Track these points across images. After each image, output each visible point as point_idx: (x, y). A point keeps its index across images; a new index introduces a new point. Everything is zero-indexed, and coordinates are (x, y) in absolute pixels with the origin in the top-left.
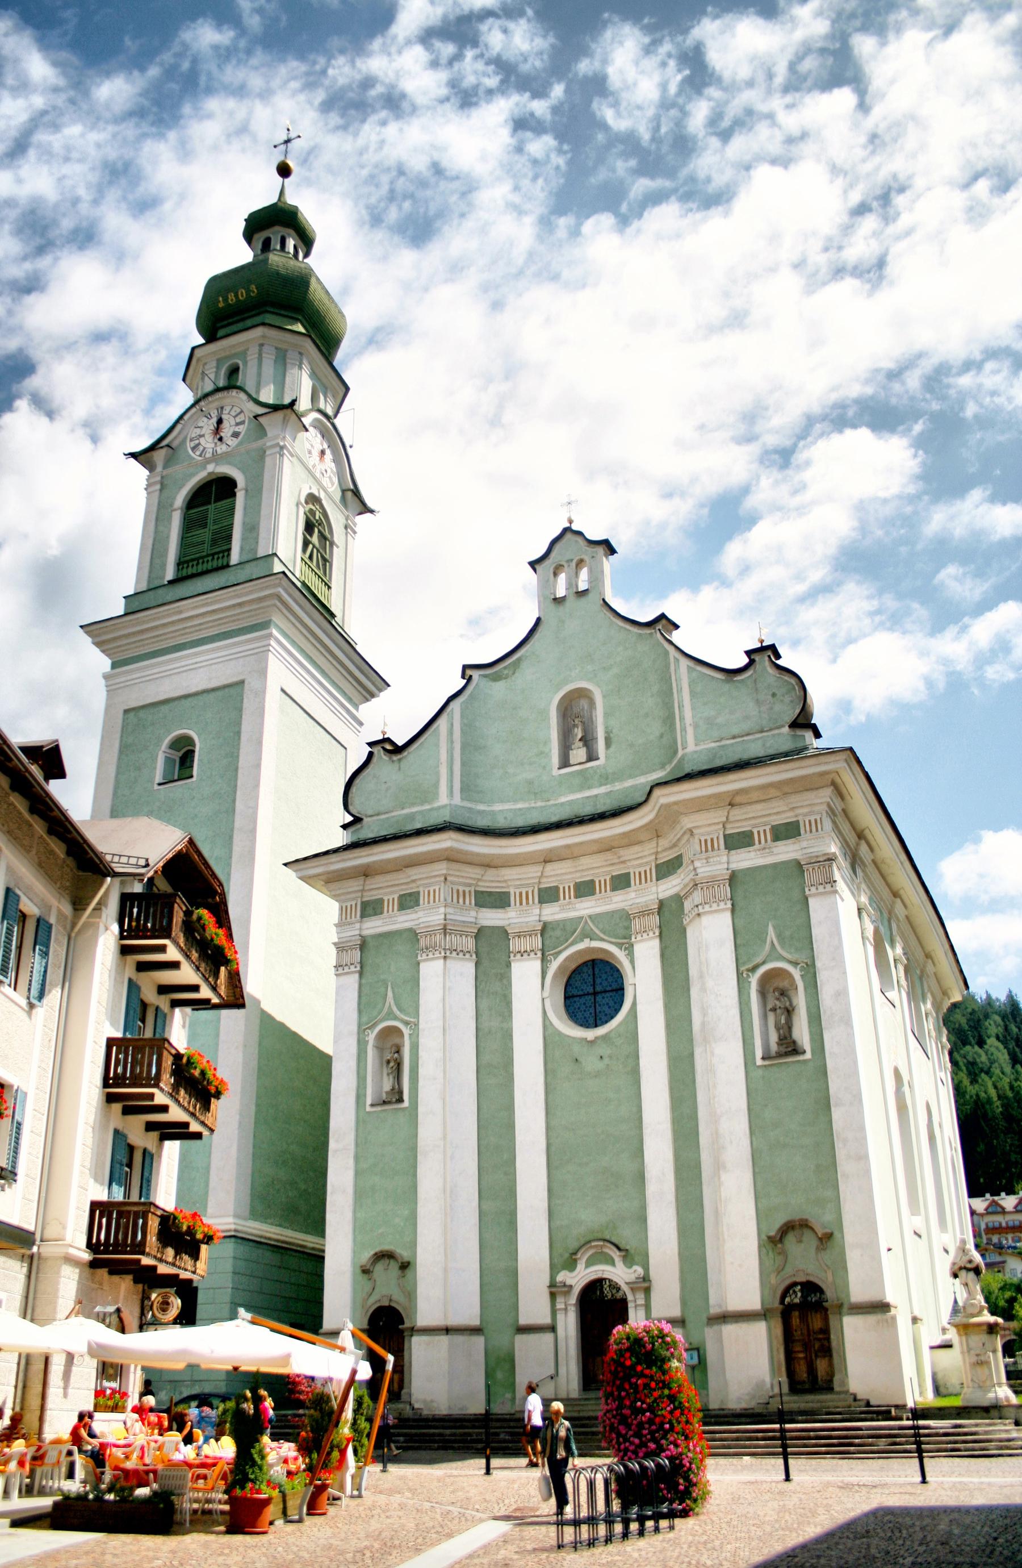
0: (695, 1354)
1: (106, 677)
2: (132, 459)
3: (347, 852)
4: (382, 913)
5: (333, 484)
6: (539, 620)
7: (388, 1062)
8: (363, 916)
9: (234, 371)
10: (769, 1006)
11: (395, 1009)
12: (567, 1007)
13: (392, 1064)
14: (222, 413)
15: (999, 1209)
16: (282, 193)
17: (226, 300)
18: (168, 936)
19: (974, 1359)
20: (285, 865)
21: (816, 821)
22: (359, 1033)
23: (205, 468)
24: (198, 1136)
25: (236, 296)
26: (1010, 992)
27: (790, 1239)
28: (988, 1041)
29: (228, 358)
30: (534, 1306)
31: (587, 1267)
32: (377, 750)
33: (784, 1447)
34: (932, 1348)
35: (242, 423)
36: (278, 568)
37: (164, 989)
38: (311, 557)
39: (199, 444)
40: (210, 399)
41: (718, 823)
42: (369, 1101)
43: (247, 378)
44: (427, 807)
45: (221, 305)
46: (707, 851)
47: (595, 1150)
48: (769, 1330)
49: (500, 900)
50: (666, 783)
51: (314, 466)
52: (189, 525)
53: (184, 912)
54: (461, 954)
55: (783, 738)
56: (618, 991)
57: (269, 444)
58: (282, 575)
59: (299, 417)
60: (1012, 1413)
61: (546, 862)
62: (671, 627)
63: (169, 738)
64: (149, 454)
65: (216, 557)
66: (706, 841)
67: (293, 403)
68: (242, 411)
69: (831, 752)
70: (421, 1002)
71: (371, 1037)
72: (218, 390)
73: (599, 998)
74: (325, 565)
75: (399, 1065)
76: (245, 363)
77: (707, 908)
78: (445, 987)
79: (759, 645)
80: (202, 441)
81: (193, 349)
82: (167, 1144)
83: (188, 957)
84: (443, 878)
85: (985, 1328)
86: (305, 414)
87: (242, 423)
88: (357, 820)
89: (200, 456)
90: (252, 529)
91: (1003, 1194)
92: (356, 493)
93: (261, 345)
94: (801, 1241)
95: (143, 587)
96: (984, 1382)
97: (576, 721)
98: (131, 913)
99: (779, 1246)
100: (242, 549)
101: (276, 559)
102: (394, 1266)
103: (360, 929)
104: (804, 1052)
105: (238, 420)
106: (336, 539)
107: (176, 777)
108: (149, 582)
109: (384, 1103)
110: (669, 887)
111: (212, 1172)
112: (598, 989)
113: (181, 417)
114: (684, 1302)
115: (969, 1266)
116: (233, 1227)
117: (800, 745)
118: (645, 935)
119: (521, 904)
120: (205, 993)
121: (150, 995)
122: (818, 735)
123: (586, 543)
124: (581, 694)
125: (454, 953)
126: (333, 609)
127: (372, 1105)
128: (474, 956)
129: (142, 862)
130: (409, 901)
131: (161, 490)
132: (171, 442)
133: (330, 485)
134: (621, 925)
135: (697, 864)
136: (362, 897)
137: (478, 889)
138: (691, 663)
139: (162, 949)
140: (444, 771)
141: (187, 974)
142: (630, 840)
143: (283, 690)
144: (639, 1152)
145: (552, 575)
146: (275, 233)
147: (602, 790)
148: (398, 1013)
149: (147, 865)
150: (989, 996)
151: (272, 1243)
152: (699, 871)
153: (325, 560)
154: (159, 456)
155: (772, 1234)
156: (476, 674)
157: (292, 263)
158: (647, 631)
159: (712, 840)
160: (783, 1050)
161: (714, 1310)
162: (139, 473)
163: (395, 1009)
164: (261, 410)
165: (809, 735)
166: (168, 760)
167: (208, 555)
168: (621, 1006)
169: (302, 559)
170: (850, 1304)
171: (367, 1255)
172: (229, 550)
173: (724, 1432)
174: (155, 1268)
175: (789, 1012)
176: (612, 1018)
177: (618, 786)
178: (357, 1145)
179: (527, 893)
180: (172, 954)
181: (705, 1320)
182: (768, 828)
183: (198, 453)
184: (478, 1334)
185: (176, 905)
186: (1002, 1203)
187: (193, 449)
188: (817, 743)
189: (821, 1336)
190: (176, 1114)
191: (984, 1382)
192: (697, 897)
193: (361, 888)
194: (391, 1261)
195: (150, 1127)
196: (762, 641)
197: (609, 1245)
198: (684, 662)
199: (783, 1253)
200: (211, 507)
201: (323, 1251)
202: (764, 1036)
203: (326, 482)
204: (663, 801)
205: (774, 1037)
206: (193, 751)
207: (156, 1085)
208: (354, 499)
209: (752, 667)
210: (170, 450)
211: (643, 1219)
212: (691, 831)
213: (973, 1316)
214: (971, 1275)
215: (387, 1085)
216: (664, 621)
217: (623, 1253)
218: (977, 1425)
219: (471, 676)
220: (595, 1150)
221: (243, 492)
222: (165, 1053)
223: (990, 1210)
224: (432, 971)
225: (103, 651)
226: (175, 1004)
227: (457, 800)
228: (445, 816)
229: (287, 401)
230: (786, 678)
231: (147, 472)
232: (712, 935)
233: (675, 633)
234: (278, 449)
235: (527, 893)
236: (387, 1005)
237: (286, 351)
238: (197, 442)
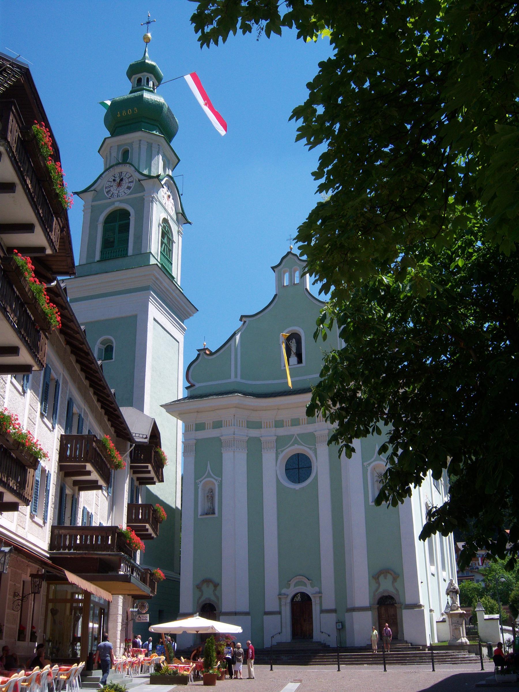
0: (340, 624)
6: (276, 295)
12: (287, 474)
13: (209, 497)
17: (121, 114)
18: (150, 462)
19: (454, 628)
20: (161, 406)
26: (296, 142)
30: (271, 604)
32: (202, 353)
33: (384, 660)
34: (437, 622)
35: (132, 182)
39: (110, 190)
42: (199, 514)
49: (258, 425)
56: (309, 468)
60: (468, 648)
68: (132, 176)
78: (234, 464)
80: (112, 189)
81: (105, 139)
87: (132, 182)
88: (192, 386)
92: (183, 214)
100: (134, 247)
101: (151, 255)
102: (211, 586)
106: (174, 239)
109: (206, 514)
112: (300, 466)
126: (173, 275)
143: (155, 319)
146: (144, 75)
156: (247, 319)
164: (142, 178)
166: (100, 350)
170: (406, 605)
173: (355, 655)
176: (306, 479)
183: (110, 195)
187: (107, 192)
197: (304, 578)
203: (170, 211)
210: (96, 193)
217: (310, 582)
218: (453, 652)
224: (227, 456)
238: (109, 189)
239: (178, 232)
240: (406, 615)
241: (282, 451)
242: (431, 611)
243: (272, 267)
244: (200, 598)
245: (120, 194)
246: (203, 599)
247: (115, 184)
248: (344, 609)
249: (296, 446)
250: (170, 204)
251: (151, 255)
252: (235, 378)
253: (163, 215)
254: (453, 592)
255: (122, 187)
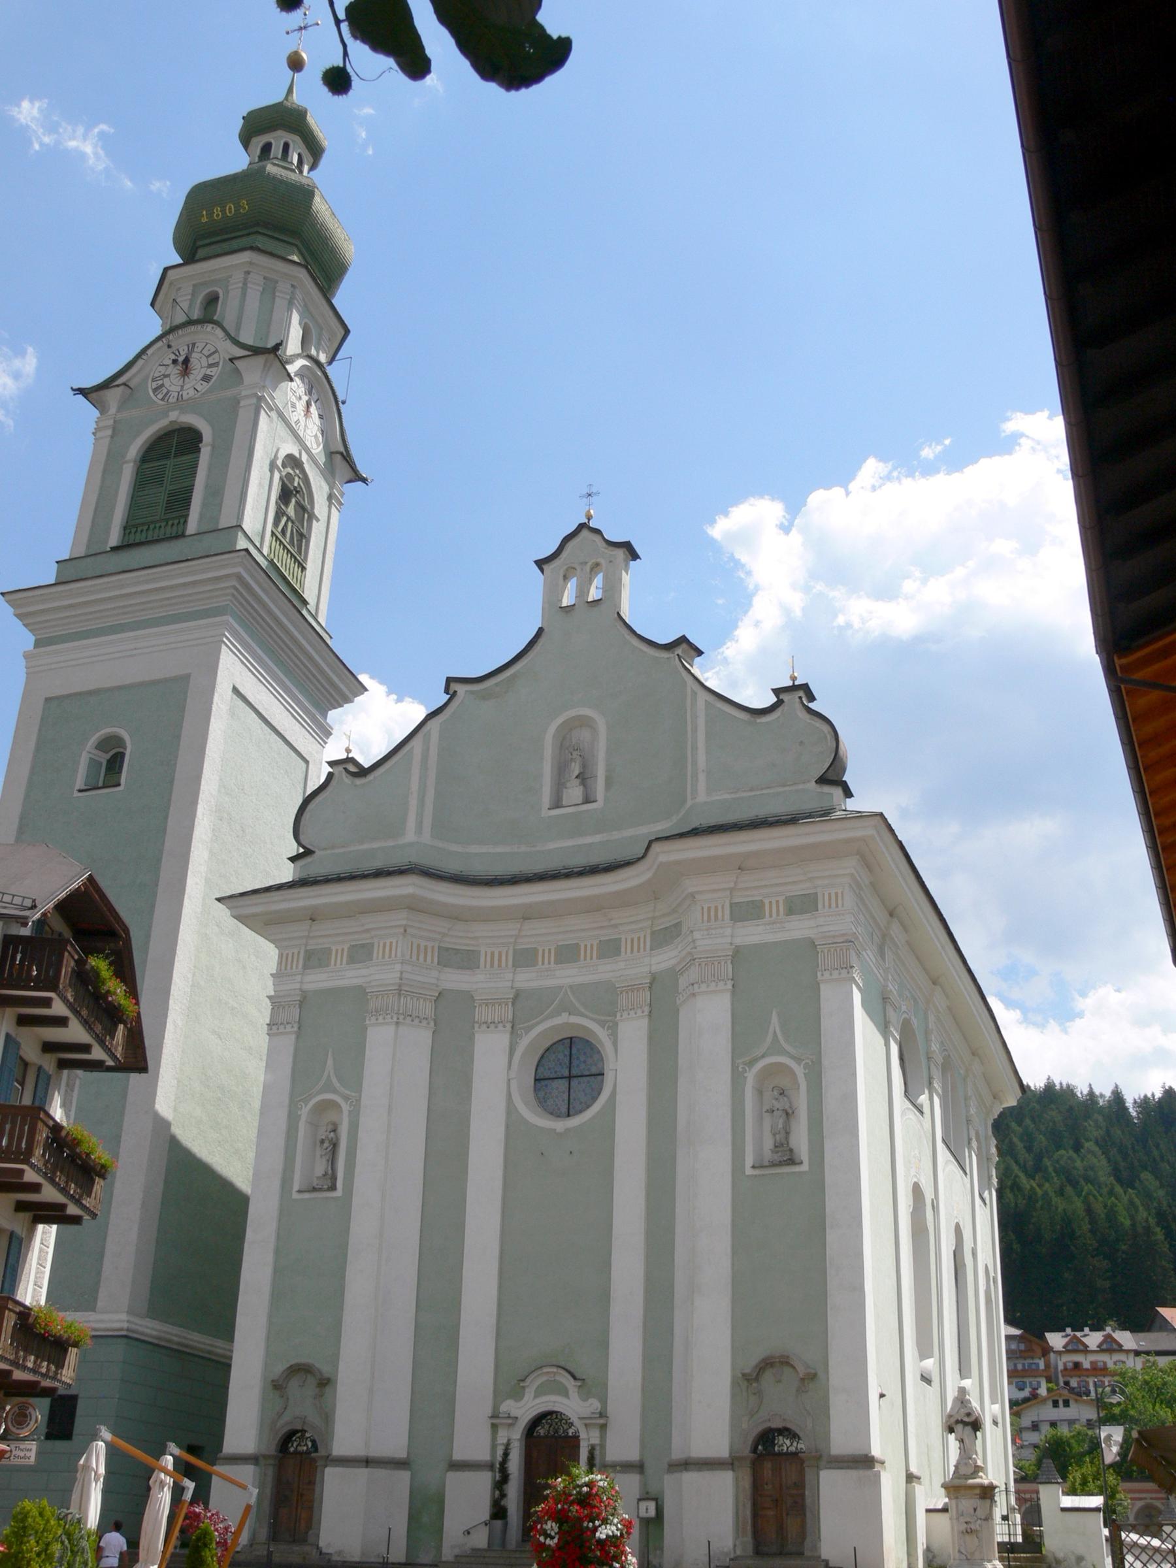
0: (652, 1506)
1: (27, 656)
2: (80, 396)
3: (291, 891)
4: (328, 965)
5: (318, 446)
6: (541, 630)
7: (322, 1142)
8: (305, 967)
9: (212, 301)
10: (766, 1108)
11: (334, 1080)
13: (326, 1144)
14: (193, 350)
15: (1081, 1348)
16: (290, 90)
17: (210, 214)
18: (54, 988)
20: (219, 900)
21: (837, 894)
22: (290, 1106)
23: (168, 416)
24: (76, 1220)
25: (223, 211)
26: (1117, 1086)
27: (768, 1377)
28: (1087, 1145)
29: (205, 284)
31: (535, 1397)
34: (928, 1511)
35: (216, 365)
36: (242, 544)
37: (48, 1047)
38: (283, 532)
39: (162, 385)
40: (180, 332)
41: (724, 889)
42: (296, 1187)
43: (227, 311)
44: (391, 843)
45: (204, 220)
46: (709, 921)
47: (556, 1257)
48: (736, 1480)
49: (467, 960)
50: (667, 838)
51: (297, 422)
52: (142, 482)
53: (76, 961)
54: (417, 1020)
55: (811, 795)
57: (244, 393)
58: (244, 553)
59: (283, 364)
61: (525, 918)
62: (693, 653)
63: (98, 735)
64: (102, 393)
65: (170, 523)
66: (709, 908)
67: (277, 347)
69: (860, 816)
70: (366, 1073)
71: (305, 1112)
72: (190, 322)
73: (574, 1082)
74: (300, 541)
75: (335, 1145)
76: (227, 292)
77: (704, 987)
78: (394, 1060)
79: (791, 684)
81: (166, 270)
82: (40, 1227)
83: (77, 1013)
84: (402, 930)
85: (978, 1491)
86: (291, 360)
87: (216, 365)
88: (308, 852)
89: (162, 399)
90: (215, 493)
91: (1087, 1329)
92: (347, 457)
93: (248, 273)
94: (779, 1381)
95: (81, 551)
96: (973, 1554)
97: (575, 753)
98: (14, 958)
99: (754, 1385)
100: (202, 516)
101: (240, 534)
102: (311, 1381)
103: (301, 982)
104: (801, 1163)
105: (211, 361)
106: (316, 512)
107: (101, 784)
108: (88, 547)
109: (314, 1190)
110: (664, 959)
111: (105, 1259)
112: (574, 1072)
113: (144, 351)
114: (643, 1445)
115: (966, 1419)
116: (125, 1325)
117: (825, 805)
118: (632, 1012)
119: (492, 965)
120: (97, 1053)
121: (31, 1052)
122: (848, 794)
123: (604, 544)
124: (583, 722)
125: (409, 1019)
127: (299, 1191)
128: (432, 1024)
129: (28, 903)
130: (360, 953)
131: (112, 437)
132: (129, 380)
133: (315, 446)
134: (605, 1001)
135: (697, 935)
136: (306, 945)
137: (442, 945)
138: (711, 698)
139: (47, 1003)
140: (413, 803)
141: (76, 1032)
142: (624, 900)
143: (235, 690)
144: (606, 1266)
145: (561, 578)
146: (277, 139)
147: (597, 838)
148: (337, 1085)
149: (34, 907)
150: (1091, 1093)
151: (175, 1347)
152: (698, 943)
153: (301, 535)
154: (113, 396)
155: (747, 1371)
156: (461, 689)
157: (293, 177)
158: (664, 655)
159: (716, 908)
160: (777, 1157)
161: (677, 1454)
162: (88, 413)
163: (334, 1080)
165: (838, 792)
167: (161, 520)
168: (599, 1094)
169: (273, 533)
171: (280, 1368)
172: (187, 516)
174: (9, 1373)
175: (788, 1114)
176: (588, 1107)
177: (616, 835)
178: (278, 1238)
179: (500, 953)
180: (59, 1008)
181: (666, 1466)
182: (781, 899)
183: (160, 396)
184: (405, 1469)
185: (66, 954)
186: (1084, 1340)
187: (155, 390)
188: (851, 805)
189: (794, 1492)
190: (49, 1194)
191: (973, 1554)
192: (693, 974)
193: (306, 933)
194: (304, 1378)
195: (21, 1207)
196: (794, 679)
198: (703, 696)
199: (759, 1393)
200: (170, 463)
201: (231, 1358)
202: (758, 1141)
203: (311, 442)
204: (662, 858)
205: (768, 1143)
206: (122, 755)
207: (26, 1161)
208: (343, 463)
209: (780, 709)
211: (604, 1345)
212: (692, 895)
213: (967, 1477)
214: (969, 1429)
215: (320, 1167)
216: (684, 646)
217: (579, 1383)
219: (455, 692)
220: (556, 1257)
221: (209, 448)
222: (40, 1124)
223: (1070, 1348)
224: (380, 1038)
225: (25, 625)
226: (63, 1064)
227: (426, 838)
228: (414, 857)
229: (271, 344)
230: (818, 725)
231: (97, 413)
232: (709, 1017)
233: (698, 660)
234: (254, 401)
235: (500, 953)
236: (326, 1073)
237: (277, 282)
238: (160, 382)
239: (330, 497)
240: (831, 1489)
241: (528, 1030)
242: (911, 1478)
243: (536, 562)
244: (280, 1415)
245: (185, 393)
246: (286, 1417)
247: (175, 371)
248: (661, 1464)
249: (563, 1018)
250: (311, 429)
251: (240, 534)
252: (415, 837)
253: (289, 448)
254: (965, 1424)
255: (191, 377)
